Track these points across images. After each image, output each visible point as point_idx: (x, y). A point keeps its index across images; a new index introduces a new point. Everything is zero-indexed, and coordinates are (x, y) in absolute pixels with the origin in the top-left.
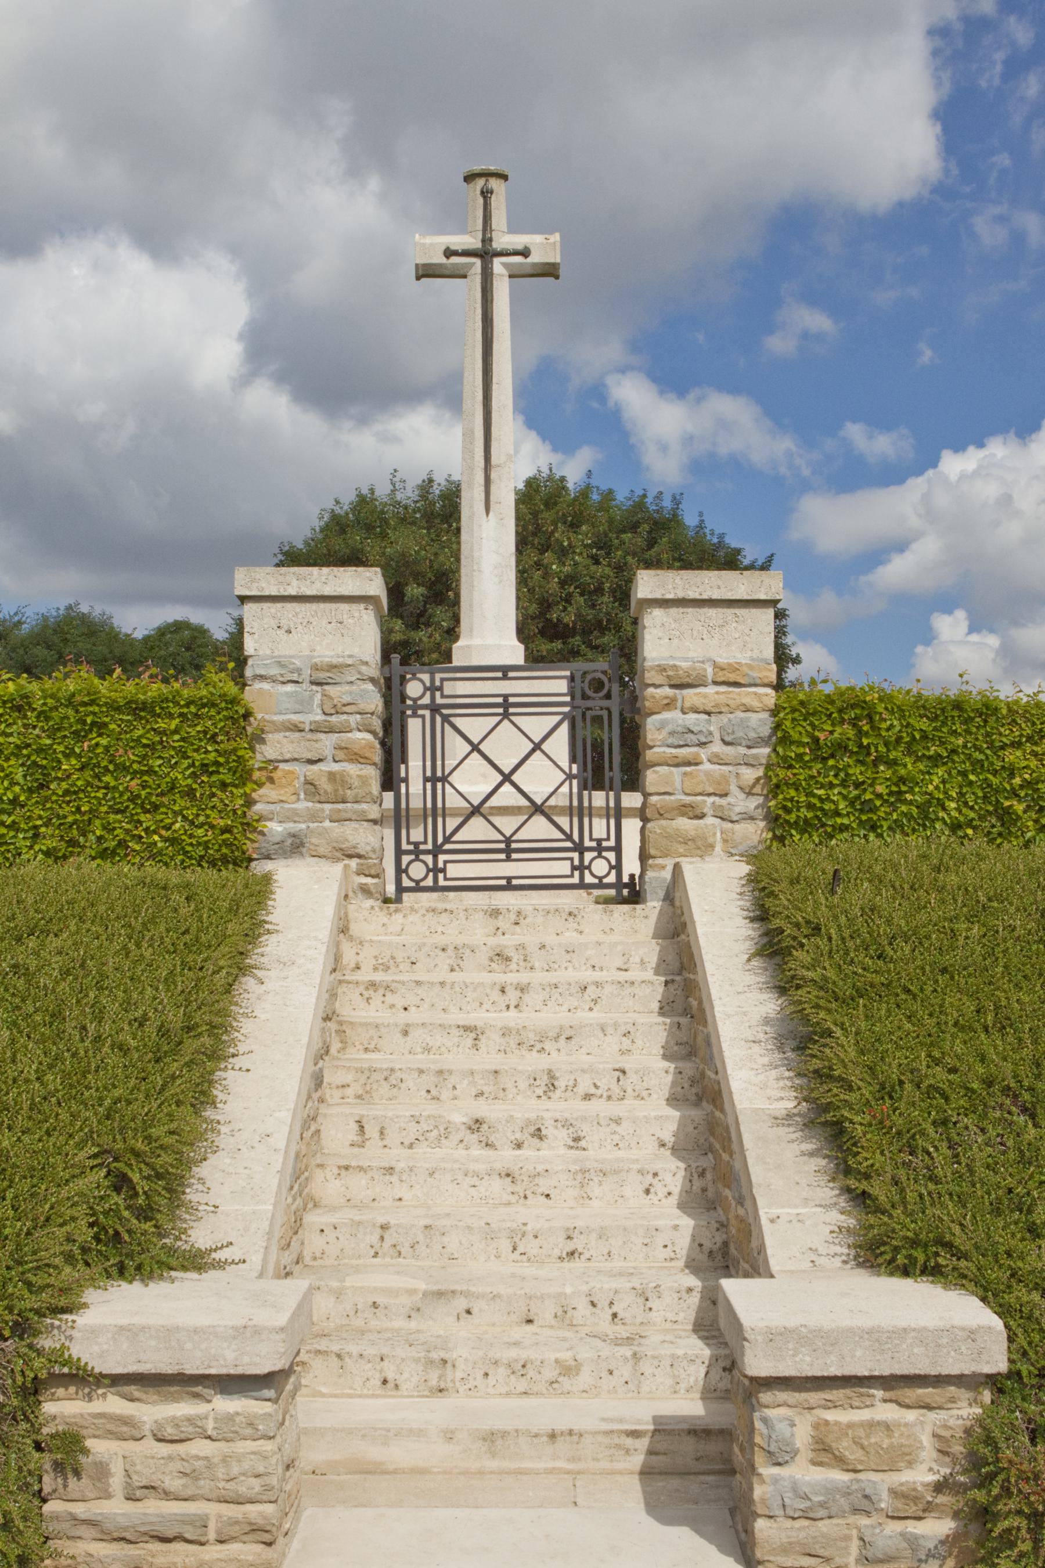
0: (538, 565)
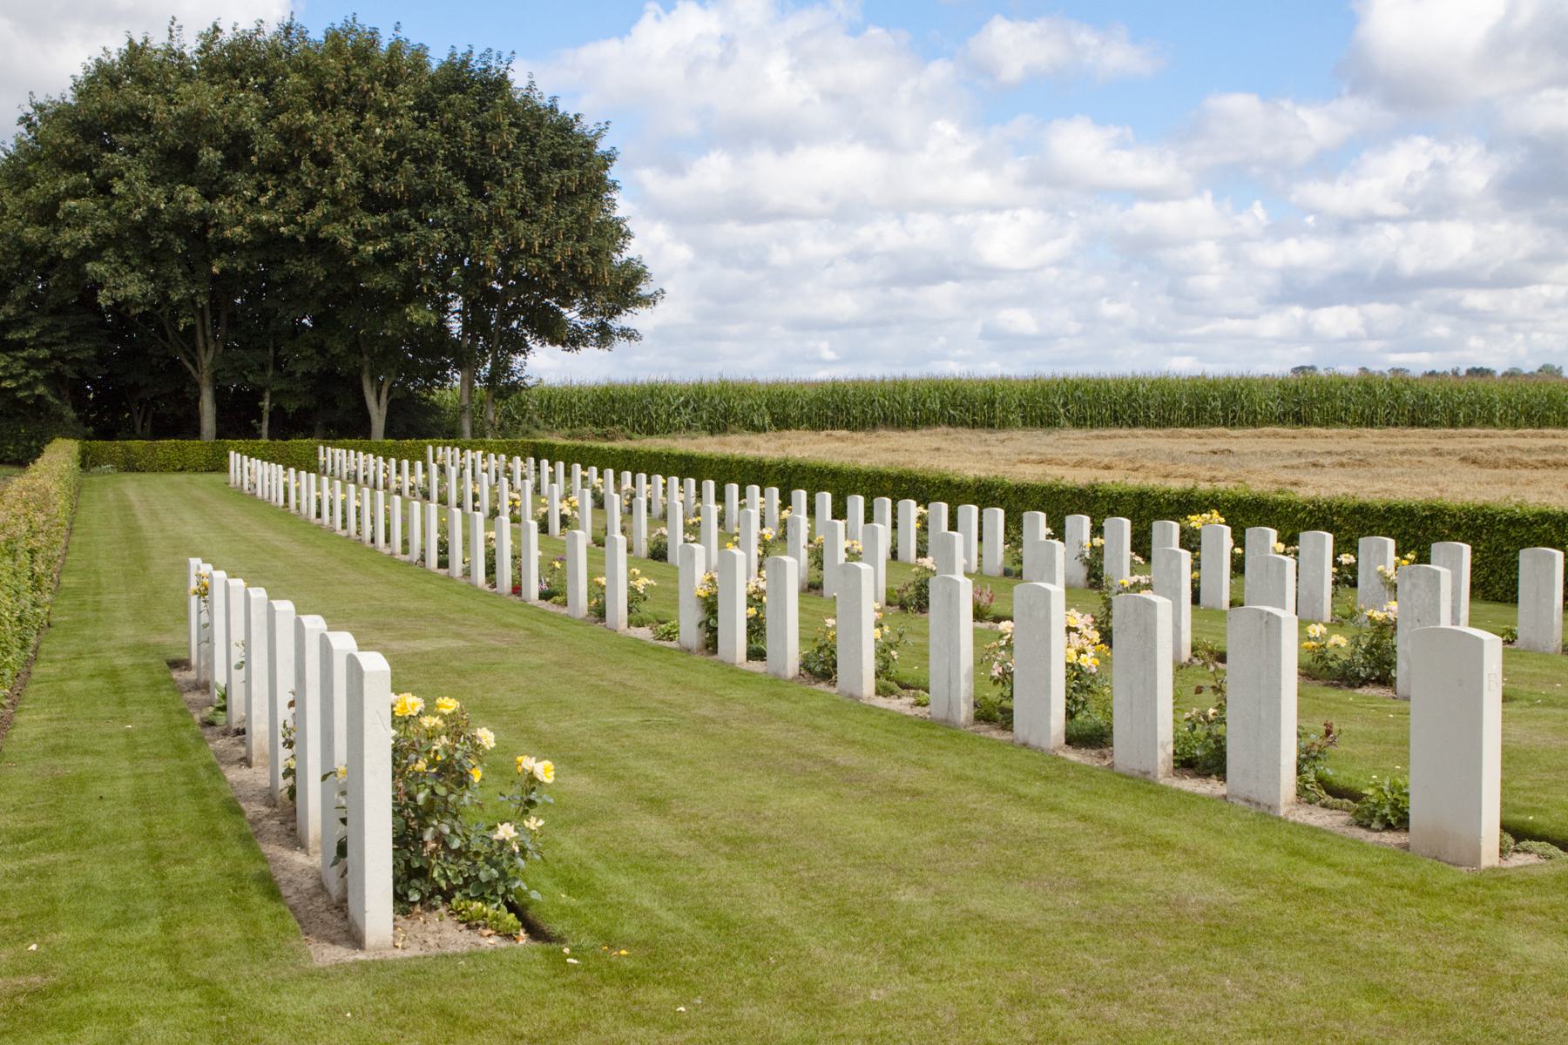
0: (356, 128)
